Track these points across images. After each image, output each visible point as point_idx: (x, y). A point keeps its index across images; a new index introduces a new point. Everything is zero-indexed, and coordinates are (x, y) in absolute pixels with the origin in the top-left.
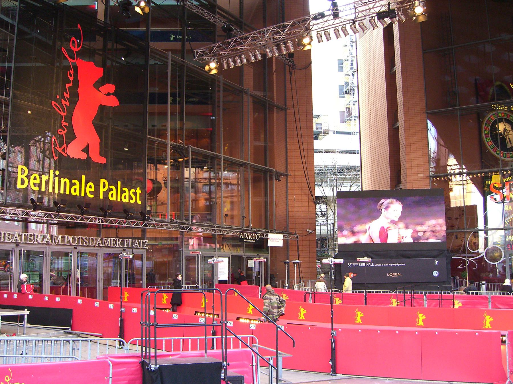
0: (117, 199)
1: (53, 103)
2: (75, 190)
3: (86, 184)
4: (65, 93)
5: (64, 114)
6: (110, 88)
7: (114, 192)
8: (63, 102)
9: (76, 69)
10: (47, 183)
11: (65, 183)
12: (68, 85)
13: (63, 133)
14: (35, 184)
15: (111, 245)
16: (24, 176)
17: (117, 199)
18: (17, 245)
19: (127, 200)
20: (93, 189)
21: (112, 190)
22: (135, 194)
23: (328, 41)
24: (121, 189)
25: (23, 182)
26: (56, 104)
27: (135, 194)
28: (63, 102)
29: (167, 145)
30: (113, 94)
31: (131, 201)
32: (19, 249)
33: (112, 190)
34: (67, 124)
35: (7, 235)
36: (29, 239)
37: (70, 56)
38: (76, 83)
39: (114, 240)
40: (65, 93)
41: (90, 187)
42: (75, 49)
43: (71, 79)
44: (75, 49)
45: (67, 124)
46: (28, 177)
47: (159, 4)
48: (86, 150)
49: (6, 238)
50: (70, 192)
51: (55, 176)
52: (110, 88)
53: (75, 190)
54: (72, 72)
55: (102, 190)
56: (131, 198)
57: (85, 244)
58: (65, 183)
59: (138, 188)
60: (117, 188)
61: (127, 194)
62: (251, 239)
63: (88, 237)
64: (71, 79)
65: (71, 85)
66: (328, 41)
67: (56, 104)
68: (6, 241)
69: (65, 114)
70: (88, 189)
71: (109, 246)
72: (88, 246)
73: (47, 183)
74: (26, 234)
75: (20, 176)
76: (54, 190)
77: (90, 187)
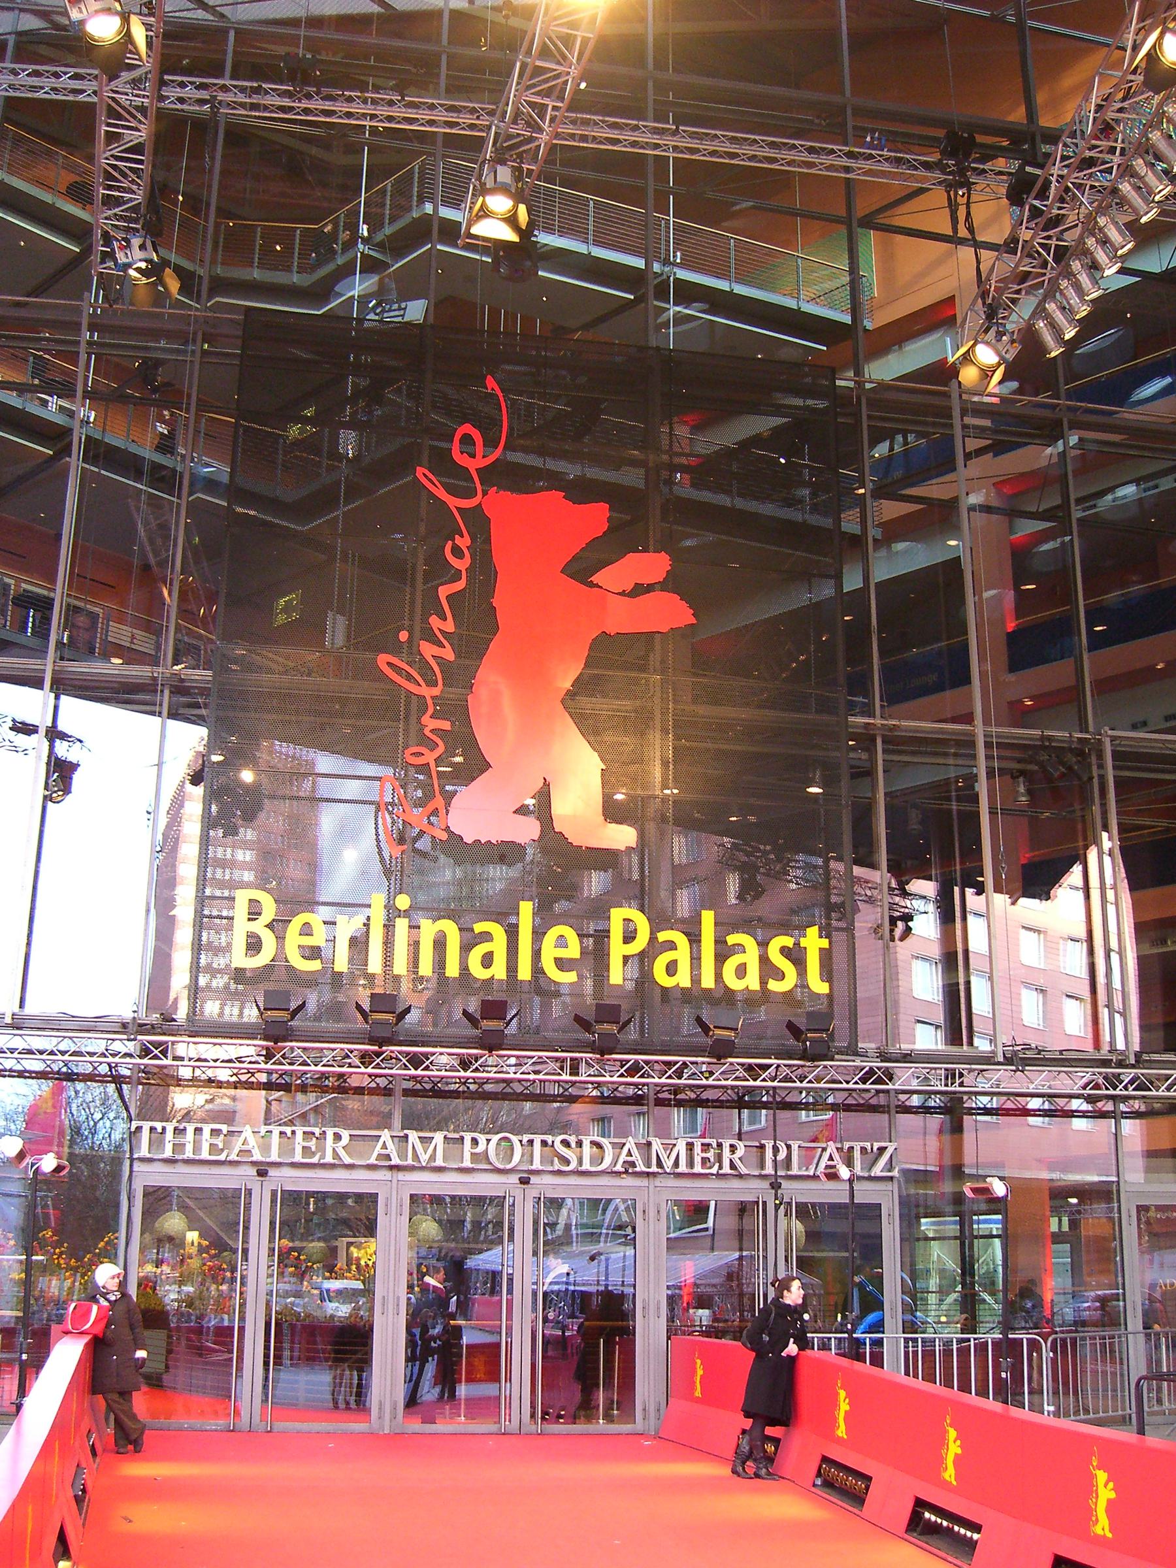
0: (512, 967)
2: (741, 971)
3: (538, 935)
4: (435, 621)
7: (682, 953)
8: (428, 650)
9: (479, 522)
10: (359, 944)
11: (440, 944)
14: (561, 964)
15: (691, 1164)
16: (259, 927)
17: (512, 967)
18: (262, 1173)
19: (752, 982)
20: (573, 951)
21: (671, 946)
22: (796, 956)
24: (720, 942)
25: (254, 945)
26: (395, 661)
27: (796, 956)
29: (972, 744)
30: (664, 586)
31: (774, 986)
32: (532, 1192)
33: (671, 946)
35: (698, 1149)
36: (299, 1150)
38: (485, 573)
39: (215, 1133)
40: (435, 621)
41: (561, 942)
43: (461, 565)
44: (473, 465)
46: (278, 926)
47: (1156, 269)
49: (697, 1160)
50: (719, 976)
51: (392, 913)
52: (652, 565)
53: (487, 960)
54: (463, 542)
55: (617, 949)
56: (768, 970)
57: (557, 1165)
58: (440, 944)
59: (813, 931)
60: (512, 933)
61: (751, 956)
63: (572, 1140)
64: (461, 565)
65: (461, 585)
67: (395, 661)
68: (698, 1169)
70: (549, 952)
71: (683, 1168)
72: (718, 1175)
73: (359, 944)
74: (159, 1126)
75: (242, 926)
76: (414, 961)
77: (561, 942)
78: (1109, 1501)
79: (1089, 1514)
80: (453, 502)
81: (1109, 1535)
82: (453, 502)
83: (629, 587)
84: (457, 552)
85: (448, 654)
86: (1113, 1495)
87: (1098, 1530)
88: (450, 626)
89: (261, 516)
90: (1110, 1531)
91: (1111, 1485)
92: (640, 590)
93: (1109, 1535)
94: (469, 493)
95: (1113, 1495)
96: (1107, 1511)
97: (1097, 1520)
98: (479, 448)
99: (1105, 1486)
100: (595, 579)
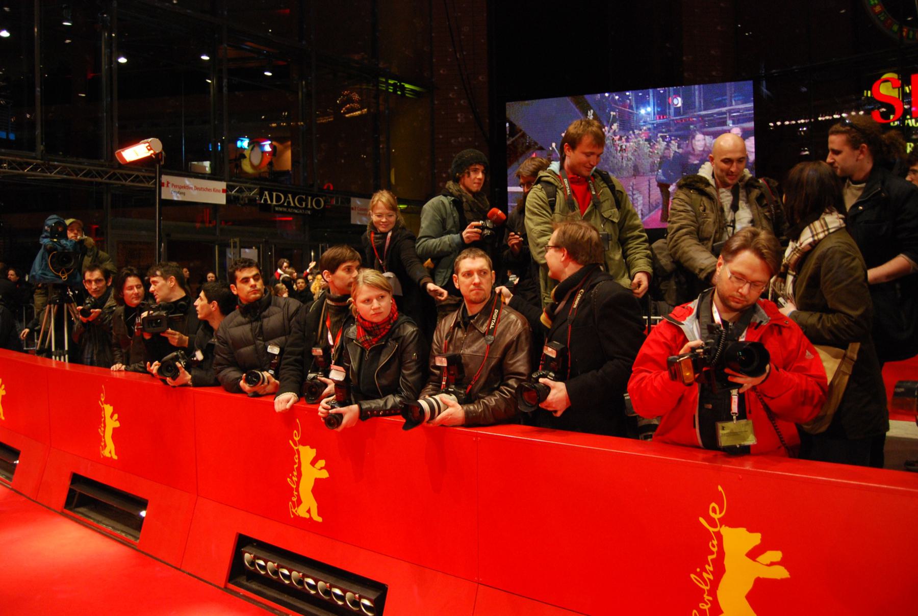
1: (693, 576)
4: (707, 567)
5: (706, 588)
6: (322, 463)
9: (719, 536)
12: (710, 558)
13: (706, 607)
23: (76, 479)
28: (705, 575)
34: (711, 598)
37: (710, 525)
40: (707, 567)
42: (297, 439)
43: (715, 550)
44: (717, 516)
45: (711, 598)
48: (309, 511)
52: (777, 555)
54: (715, 542)
62: (296, 207)
64: (715, 550)
65: (714, 556)
66: (76, 479)
69: (708, 588)
78: (115, 430)
79: (98, 440)
80: (711, 529)
81: (115, 457)
82: (711, 529)
83: (768, 563)
84: (713, 546)
85: (711, 577)
86: (117, 424)
87: (106, 453)
88: (711, 569)
89: (37, 42)
90: (116, 454)
91: (116, 416)
92: (772, 564)
93: (115, 457)
94: (716, 526)
95: (117, 424)
96: (113, 437)
97: (105, 446)
98: (718, 511)
99: (112, 417)
100: (759, 559)
